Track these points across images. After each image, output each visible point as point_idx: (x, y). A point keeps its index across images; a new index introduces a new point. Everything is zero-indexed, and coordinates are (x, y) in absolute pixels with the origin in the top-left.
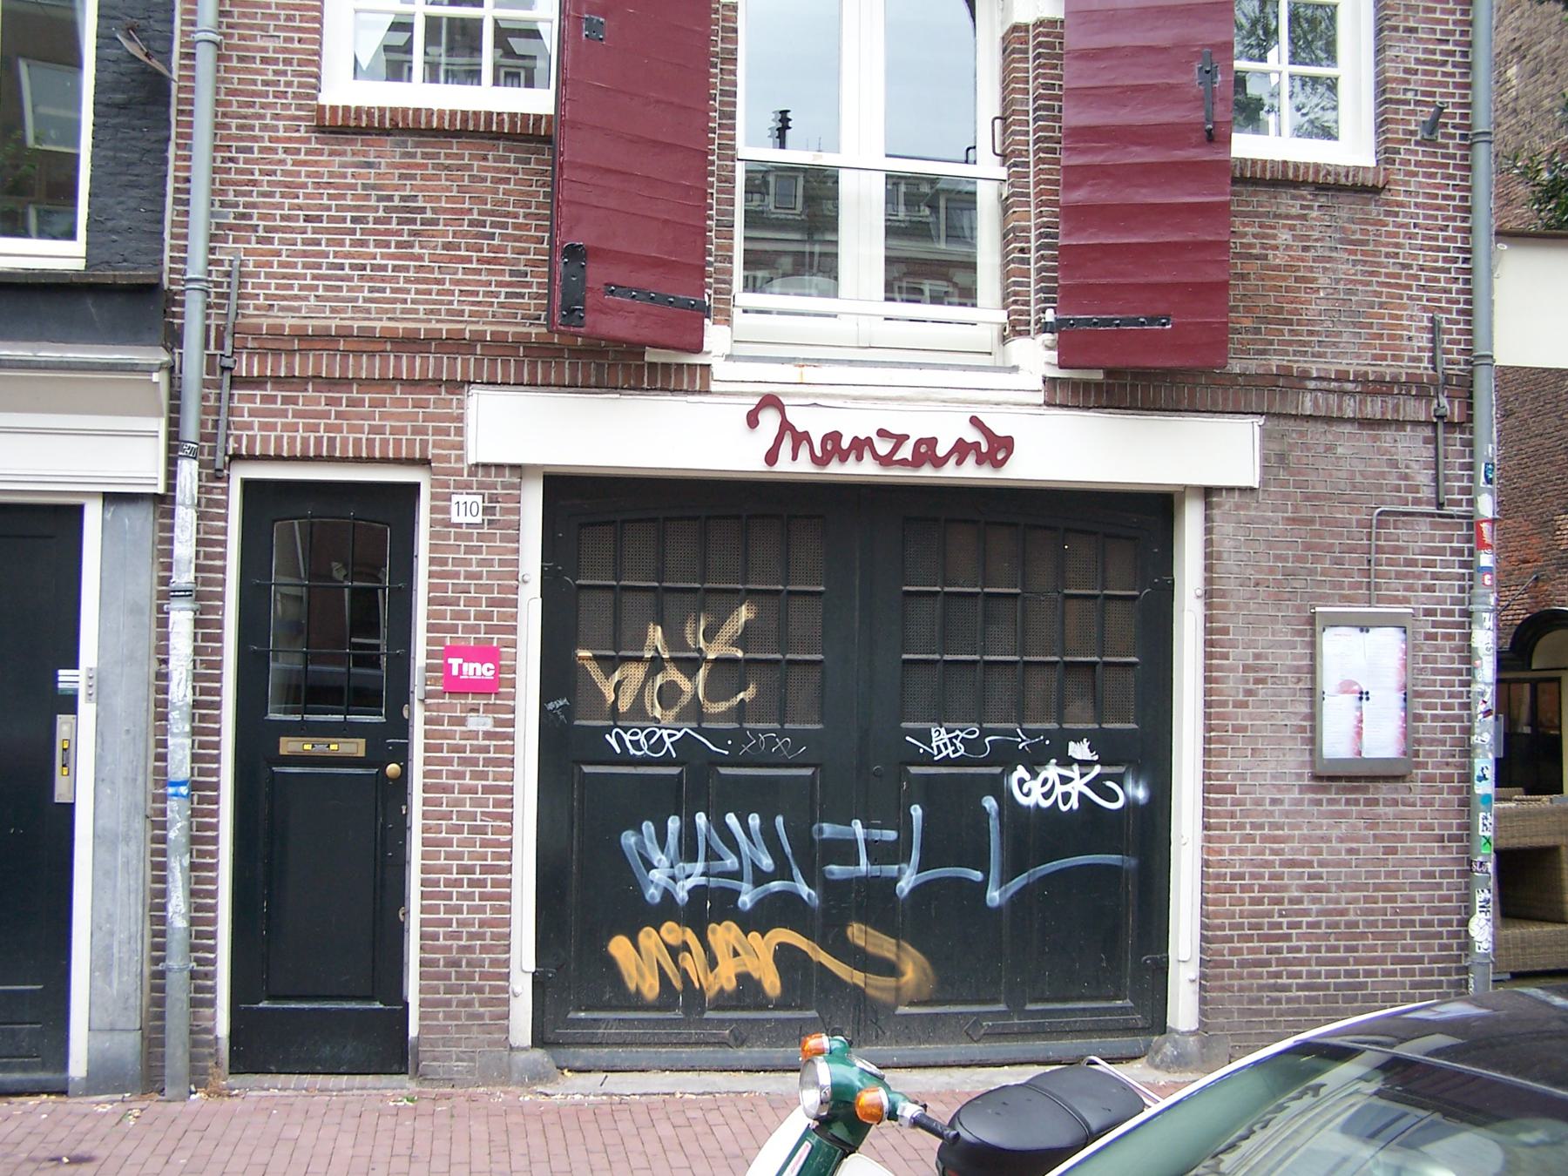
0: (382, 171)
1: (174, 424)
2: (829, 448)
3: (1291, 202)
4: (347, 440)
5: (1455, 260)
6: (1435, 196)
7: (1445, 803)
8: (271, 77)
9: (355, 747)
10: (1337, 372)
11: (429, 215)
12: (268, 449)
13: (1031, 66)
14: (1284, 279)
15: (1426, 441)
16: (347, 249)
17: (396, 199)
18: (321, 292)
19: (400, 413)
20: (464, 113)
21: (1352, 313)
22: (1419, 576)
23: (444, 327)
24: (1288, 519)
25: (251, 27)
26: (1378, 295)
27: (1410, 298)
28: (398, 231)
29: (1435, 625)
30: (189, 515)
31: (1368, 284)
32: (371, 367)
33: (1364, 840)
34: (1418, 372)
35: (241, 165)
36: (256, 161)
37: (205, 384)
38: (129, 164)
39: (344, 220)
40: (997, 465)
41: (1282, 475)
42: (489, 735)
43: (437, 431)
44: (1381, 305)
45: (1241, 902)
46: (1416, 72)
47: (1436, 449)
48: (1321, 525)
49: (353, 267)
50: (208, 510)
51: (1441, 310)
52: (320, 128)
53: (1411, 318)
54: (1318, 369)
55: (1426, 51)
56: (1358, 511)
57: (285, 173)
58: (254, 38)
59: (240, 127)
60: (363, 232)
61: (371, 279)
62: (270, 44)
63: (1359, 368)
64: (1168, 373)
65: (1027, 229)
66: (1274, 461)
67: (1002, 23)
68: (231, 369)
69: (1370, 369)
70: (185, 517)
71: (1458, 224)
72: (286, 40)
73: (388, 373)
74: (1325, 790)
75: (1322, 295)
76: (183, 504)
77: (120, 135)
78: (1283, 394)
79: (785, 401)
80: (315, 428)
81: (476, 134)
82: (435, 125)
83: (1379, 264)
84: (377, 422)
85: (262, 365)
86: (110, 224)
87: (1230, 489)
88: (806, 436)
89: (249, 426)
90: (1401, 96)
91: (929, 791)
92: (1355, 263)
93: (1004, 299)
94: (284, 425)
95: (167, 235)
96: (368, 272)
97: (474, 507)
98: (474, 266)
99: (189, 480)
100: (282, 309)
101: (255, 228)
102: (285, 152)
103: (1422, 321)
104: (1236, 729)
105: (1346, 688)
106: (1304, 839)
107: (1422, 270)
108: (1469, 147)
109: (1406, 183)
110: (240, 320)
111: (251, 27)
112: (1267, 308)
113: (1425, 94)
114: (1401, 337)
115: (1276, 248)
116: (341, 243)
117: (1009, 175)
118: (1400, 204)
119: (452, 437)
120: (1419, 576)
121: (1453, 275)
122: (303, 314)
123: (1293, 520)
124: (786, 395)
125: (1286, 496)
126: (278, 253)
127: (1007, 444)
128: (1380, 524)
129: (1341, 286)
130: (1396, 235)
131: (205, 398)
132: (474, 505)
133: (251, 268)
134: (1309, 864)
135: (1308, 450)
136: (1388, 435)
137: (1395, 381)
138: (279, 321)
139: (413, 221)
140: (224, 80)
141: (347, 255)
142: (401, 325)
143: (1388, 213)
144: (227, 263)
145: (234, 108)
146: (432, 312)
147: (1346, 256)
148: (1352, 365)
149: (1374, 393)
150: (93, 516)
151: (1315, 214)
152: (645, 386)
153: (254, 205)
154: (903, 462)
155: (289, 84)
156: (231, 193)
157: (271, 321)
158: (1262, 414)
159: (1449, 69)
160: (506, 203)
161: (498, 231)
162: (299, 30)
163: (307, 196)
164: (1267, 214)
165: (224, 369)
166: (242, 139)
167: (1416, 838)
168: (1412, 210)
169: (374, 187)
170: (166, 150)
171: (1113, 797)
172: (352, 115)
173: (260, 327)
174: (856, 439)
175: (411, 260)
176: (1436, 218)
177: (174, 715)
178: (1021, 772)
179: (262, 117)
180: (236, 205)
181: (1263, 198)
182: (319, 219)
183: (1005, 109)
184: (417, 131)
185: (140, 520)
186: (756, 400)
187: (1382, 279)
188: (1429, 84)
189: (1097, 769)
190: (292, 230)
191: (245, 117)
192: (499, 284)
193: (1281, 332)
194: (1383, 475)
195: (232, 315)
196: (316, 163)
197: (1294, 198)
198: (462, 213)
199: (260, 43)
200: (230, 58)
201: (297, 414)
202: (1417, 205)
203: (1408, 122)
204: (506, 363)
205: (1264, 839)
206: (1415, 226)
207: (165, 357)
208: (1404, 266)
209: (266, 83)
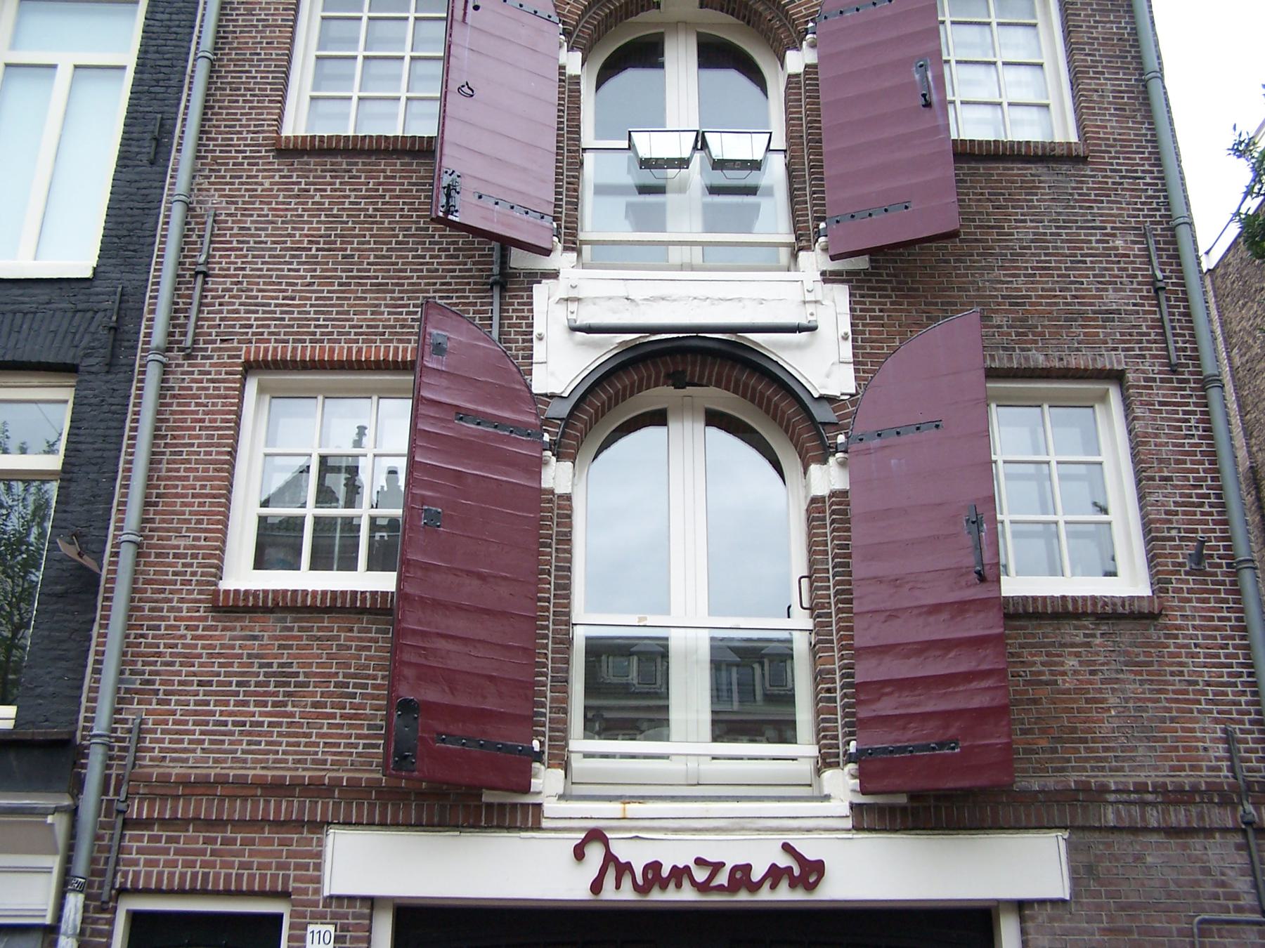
0: (264, 643)
1: (68, 861)
2: (650, 876)
3: (1075, 632)
4: (219, 875)
5: (1240, 675)
6: (1212, 619)
8: (180, 569)
10: (1135, 784)
11: (301, 679)
12: (150, 883)
13: (828, 531)
14: (1075, 700)
15: (1239, 847)
16: (231, 708)
17: (275, 666)
18: (206, 746)
19: (267, 851)
20: (334, 593)
21: (1144, 729)
23: (307, 774)
24: (1104, 930)
25: (168, 530)
26: (1169, 710)
27: (1199, 711)
28: (274, 692)
30: (69, 944)
31: (1158, 700)
32: (244, 809)
34: (1218, 780)
35: (150, 640)
36: (162, 637)
38: (61, 641)
39: (230, 684)
40: (811, 887)
41: (1093, 886)
43: (298, 867)
44: (1172, 720)
46: (1176, 513)
47: (1251, 856)
48: (1139, 934)
49: (235, 724)
51: (1233, 721)
52: (216, 608)
53: (1204, 730)
54: (1115, 783)
55: (1182, 495)
56: (1177, 920)
57: (185, 646)
58: (169, 538)
59: (151, 609)
60: (246, 694)
61: (250, 733)
62: (182, 543)
63: (1157, 779)
64: (967, 793)
65: (833, 672)
66: (1081, 873)
67: (806, 497)
68: (124, 812)
69: (1168, 780)
71: (1237, 642)
72: (195, 539)
73: (258, 816)
75: (1113, 713)
76: (65, 934)
77: (55, 618)
78: (1085, 809)
79: (609, 835)
80: (192, 864)
81: (342, 609)
82: (309, 604)
83: (1166, 683)
84: (246, 859)
85: (151, 809)
86: (39, 690)
87: (1042, 902)
88: (628, 866)
89: (135, 863)
90: (1166, 534)
92: (1142, 682)
93: (818, 735)
94: (165, 861)
95: (84, 699)
96: (247, 728)
97: (327, 935)
98: (337, 721)
99: (72, 913)
100: (173, 760)
101: (156, 692)
102: (186, 629)
103: (1215, 732)
107: (1209, 685)
108: (1236, 574)
109: (1182, 609)
110: (137, 770)
111: (168, 530)
112: (1061, 728)
113: (1187, 531)
114: (1197, 749)
115: (1064, 673)
116: (227, 704)
117: (815, 626)
118: (1179, 628)
119: (311, 872)
121: (1240, 688)
122: (190, 764)
124: (612, 829)
125: (1099, 907)
126: (174, 713)
127: (818, 868)
128: (1202, 933)
129: (1131, 705)
131: (98, 837)
132: (327, 934)
133: (150, 726)
135: (1117, 860)
136: (1197, 843)
137: (1195, 790)
138: (167, 770)
139: (288, 684)
140: (143, 572)
141: (231, 714)
142: (269, 773)
143: (1168, 636)
144: (130, 721)
145: (148, 595)
146: (299, 761)
147: (1132, 677)
148: (1149, 777)
149: (1176, 803)
151: (1098, 641)
152: (483, 824)
153: (157, 673)
154: (720, 888)
155: (194, 574)
156: (140, 663)
157: (161, 770)
158: (1066, 828)
159: (1207, 509)
160: (367, 667)
161: (359, 691)
162: (206, 530)
163: (201, 665)
164: (1052, 644)
165: (120, 812)
166: (152, 619)
168: (1191, 632)
169: (257, 656)
170: (91, 630)
172: (242, 597)
173: (151, 775)
174: (675, 867)
175: (284, 717)
176: (1215, 638)
179: (171, 601)
180: (143, 673)
181: (1049, 630)
182: (210, 683)
183: (810, 568)
184: (293, 609)
186: (583, 835)
187: (1171, 696)
188: (1190, 522)
190: (187, 693)
191: (156, 601)
192: (358, 737)
193: (1077, 750)
194: (1197, 883)
195: (129, 766)
196: (211, 637)
197: (1076, 628)
198: (329, 677)
199: (174, 542)
200: (149, 555)
201: (177, 852)
202: (1194, 627)
203: (1176, 556)
204: (360, 806)
206: (1196, 645)
207: (66, 801)
208: (1190, 683)
209: (175, 574)
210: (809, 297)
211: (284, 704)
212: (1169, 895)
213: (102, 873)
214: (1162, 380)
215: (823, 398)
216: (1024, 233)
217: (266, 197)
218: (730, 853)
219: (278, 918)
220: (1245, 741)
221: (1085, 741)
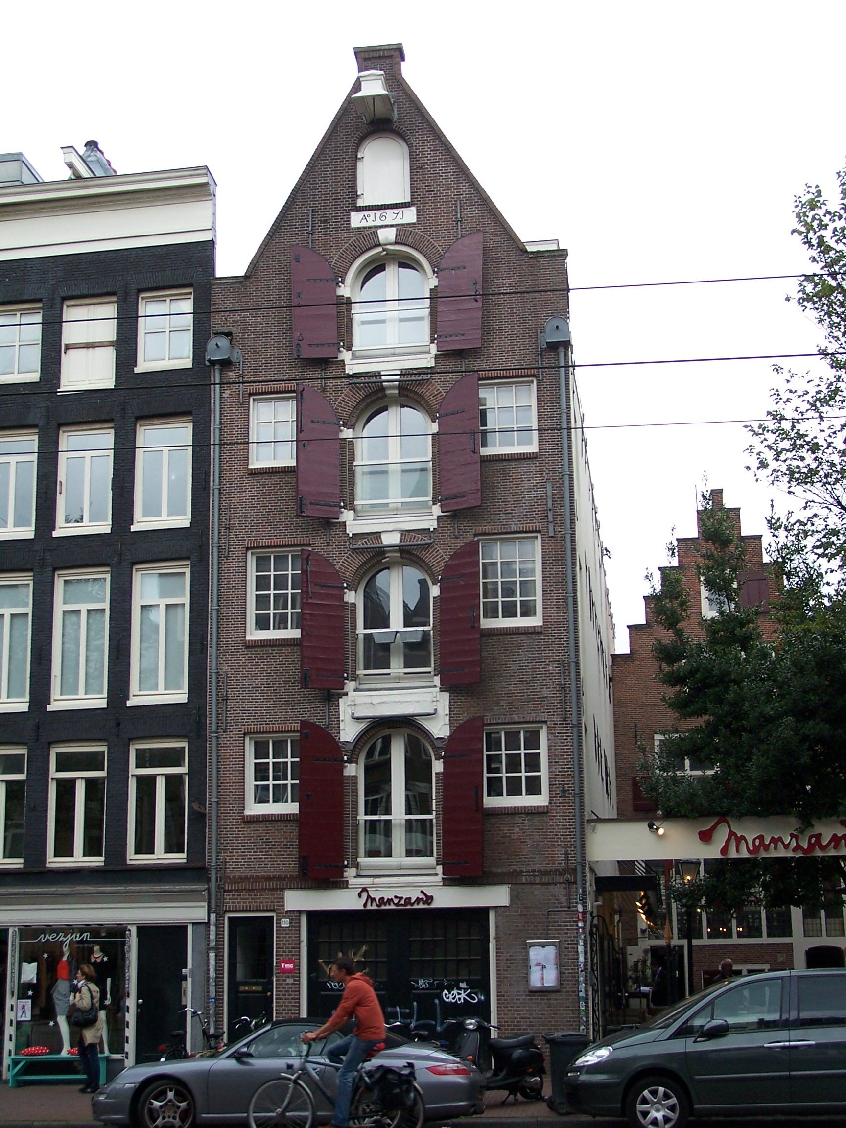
1: (209, 906)
4: (254, 905)
7: (574, 999)
9: (260, 988)
22: (563, 930)
26: (547, 844)
29: (568, 944)
33: (547, 1011)
37: (217, 892)
40: (429, 904)
42: (292, 984)
43: (277, 902)
44: (548, 848)
45: (508, 1030)
50: (219, 926)
66: (513, 897)
70: (213, 928)
74: (534, 996)
79: (369, 889)
80: (245, 902)
89: (229, 903)
91: (418, 998)
101: (228, 849)
104: (504, 978)
105: (538, 964)
106: (527, 1011)
118: (554, 816)
120: (563, 930)
123: (521, 915)
126: (234, 856)
127: (431, 898)
130: (553, 826)
131: (217, 896)
134: (529, 1018)
136: (551, 887)
148: (537, 867)
150: (190, 929)
167: (564, 1010)
171: (474, 999)
177: (211, 980)
178: (446, 992)
185: (202, 929)
186: (360, 890)
189: (469, 991)
201: (241, 899)
205: (514, 1011)
210: (435, 699)
211: (268, 852)
212: (541, 904)
213: (219, 906)
214: (560, 724)
215: (438, 738)
216: (514, 667)
217: (244, 666)
218: (405, 893)
219: (273, 916)
220: (571, 854)
221: (518, 855)
